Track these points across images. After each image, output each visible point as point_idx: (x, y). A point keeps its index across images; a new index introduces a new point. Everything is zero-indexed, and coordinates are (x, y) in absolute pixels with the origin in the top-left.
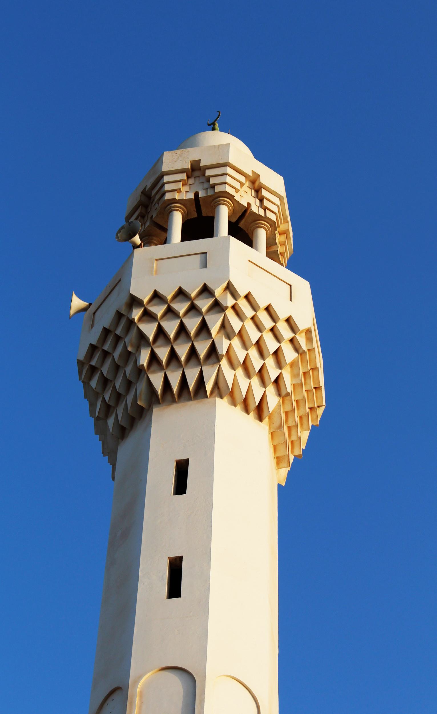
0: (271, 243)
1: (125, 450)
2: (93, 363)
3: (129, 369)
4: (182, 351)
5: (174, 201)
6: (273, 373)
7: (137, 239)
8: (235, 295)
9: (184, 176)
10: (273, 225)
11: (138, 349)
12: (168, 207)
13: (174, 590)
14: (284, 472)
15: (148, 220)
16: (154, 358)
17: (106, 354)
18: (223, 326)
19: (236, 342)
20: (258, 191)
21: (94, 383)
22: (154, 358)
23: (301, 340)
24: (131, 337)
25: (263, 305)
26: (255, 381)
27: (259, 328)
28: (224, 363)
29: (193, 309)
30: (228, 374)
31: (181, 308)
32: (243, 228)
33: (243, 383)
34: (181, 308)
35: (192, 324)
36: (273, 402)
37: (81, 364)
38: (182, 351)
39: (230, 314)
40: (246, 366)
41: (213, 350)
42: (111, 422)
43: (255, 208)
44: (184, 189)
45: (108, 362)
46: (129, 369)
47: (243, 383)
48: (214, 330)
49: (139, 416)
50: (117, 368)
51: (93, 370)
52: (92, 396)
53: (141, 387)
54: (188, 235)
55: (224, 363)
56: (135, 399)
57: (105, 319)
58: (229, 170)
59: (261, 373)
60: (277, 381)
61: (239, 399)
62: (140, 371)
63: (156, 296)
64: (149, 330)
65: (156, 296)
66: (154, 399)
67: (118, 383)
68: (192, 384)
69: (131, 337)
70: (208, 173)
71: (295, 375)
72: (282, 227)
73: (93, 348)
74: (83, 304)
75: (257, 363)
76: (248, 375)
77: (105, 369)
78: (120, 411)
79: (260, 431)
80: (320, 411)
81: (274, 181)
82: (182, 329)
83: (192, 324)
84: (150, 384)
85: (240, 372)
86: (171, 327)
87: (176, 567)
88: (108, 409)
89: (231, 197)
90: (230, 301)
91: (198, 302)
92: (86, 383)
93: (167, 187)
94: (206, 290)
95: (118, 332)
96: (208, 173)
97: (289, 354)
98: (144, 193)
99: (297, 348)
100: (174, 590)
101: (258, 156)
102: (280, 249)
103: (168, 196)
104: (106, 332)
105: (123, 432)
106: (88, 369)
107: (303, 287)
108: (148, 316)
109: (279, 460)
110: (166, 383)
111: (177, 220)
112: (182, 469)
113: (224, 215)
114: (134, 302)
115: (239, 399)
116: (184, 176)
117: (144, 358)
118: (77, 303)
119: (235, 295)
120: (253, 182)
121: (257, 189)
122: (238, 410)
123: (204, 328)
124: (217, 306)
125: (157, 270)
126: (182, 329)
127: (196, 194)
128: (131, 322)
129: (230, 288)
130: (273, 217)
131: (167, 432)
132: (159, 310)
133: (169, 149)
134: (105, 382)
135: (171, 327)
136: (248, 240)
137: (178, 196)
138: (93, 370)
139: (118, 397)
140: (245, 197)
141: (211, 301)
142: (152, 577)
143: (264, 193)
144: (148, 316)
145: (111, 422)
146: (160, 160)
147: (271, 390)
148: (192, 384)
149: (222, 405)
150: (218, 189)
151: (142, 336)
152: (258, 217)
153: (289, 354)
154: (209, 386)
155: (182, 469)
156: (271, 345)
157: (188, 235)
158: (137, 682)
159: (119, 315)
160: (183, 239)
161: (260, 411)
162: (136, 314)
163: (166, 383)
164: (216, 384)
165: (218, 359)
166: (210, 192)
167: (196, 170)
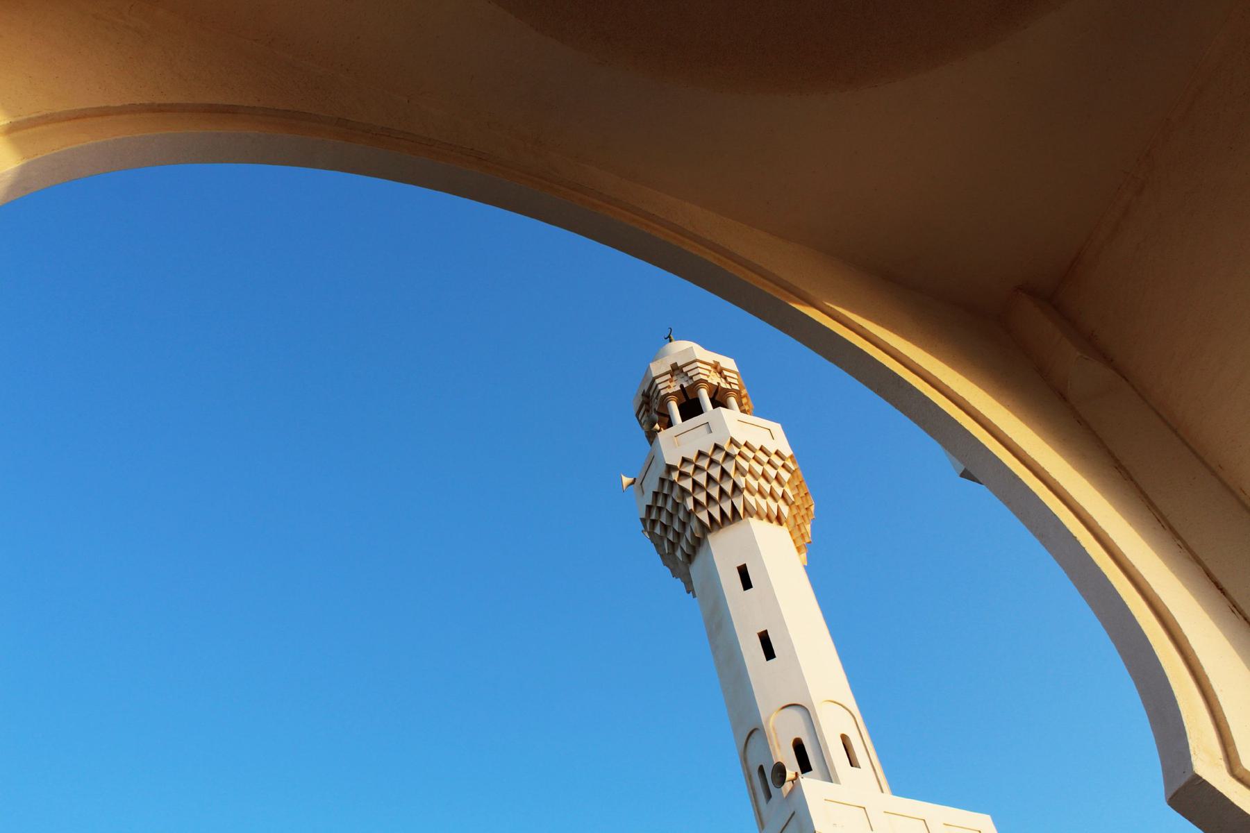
0: (740, 405)
1: (695, 570)
2: (653, 517)
3: (681, 515)
4: (715, 492)
5: (668, 394)
6: (779, 491)
7: (657, 426)
8: (737, 445)
9: (669, 376)
10: (738, 392)
11: (683, 499)
12: (664, 401)
13: (769, 653)
14: (804, 555)
15: (653, 412)
16: (696, 502)
17: (660, 509)
18: (737, 469)
19: (749, 477)
20: (720, 373)
21: (658, 530)
22: (696, 502)
23: (789, 463)
24: (676, 493)
25: (758, 447)
26: (769, 500)
27: (759, 462)
28: (746, 493)
29: (712, 462)
30: (752, 500)
31: (704, 463)
32: (719, 399)
33: (763, 503)
34: (704, 463)
35: (716, 473)
36: (785, 510)
37: (643, 521)
38: (715, 492)
39: (739, 459)
40: (760, 492)
41: (735, 486)
42: (679, 554)
43: (724, 385)
44: (672, 384)
45: (664, 514)
46: (681, 515)
47: (763, 503)
48: (732, 471)
49: (698, 543)
50: (671, 516)
51: (654, 522)
52: (657, 542)
53: (694, 524)
54: (685, 416)
55: (746, 493)
56: (693, 534)
57: (652, 485)
58: (699, 364)
59: (772, 494)
60: (783, 497)
61: (764, 515)
62: (689, 514)
63: (684, 460)
64: (687, 484)
65: (684, 460)
66: (705, 530)
67: (676, 526)
68: (717, 516)
69: (676, 493)
70: (685, 370)
71: (792, 490)
72: (744, 392)
73: (649, 508)
74: (631, 480)
75: (767, 487)
76: (764, 497)
77: (664, 519)
78: (684, 544)
79: (783, 531)
80: (812, 508)
81: (728, 363)
82: (710, 478)
83: (716, 473)
84: (700, 521)
85: (758, 496)
86: (701, 478)
87: (765, 639)
88: (673, 545)
89: (706, 381)
90: (736, 451)
91: (714, 457)
92: (652, 534)
93: (660, 387)
94: (717, 447)
95: (665, 492)
96: (685, 370)
97: (786, 476)
98: (644, 394)
99: (788, 470)
100: (769, 653)
101: (707, 347)
102: (747, 408)
103: (663, 393)
104: (656, 494)
105: (689, 558)
106: (649, 522)
107: (777, 428)
108: (683, 475)
109: (799, 549)
110: (711, 516)
111: (674, 408)
112: (743, 572)
113: (704, 395)
114: (670, 468)
115: (764, 515)
116: (669, 376)
117: (690, 504)
118: (626, 480)
119: (737, 445)
120: (715, 368)
121: (720, 371)
122: (765, 522)
123: (724, 473)
124: (728, 456)
125: (679, 442)
126: (710, 478)
127: (682, 386)
128: (673, 483)
129: (732, 441)
130: (736, 387)
131: (724, 550)
132: (689, 469)
133: (654, 360)
134: (665, 528)
135: (701, 478)
136: (725, 406)
137: (670, 391)
138: (654, 522)
139: (678, 535)
140: (715, 379)
141: (723, 454)
142: (751, 650)
143: (726, 373)
144: (683, 475)
145: (679, 554)
146: (649, 368)
147: (781, 503)
148: (717, 516)
149: (753, 521)
150: (695, 379)
151: (683, 490)
152: (727, 390)
153: (786, 476)
154: (741, 511)
155: (743, 572)
156: (772, 473)
157: (685, 416)
158: (767, 722)
159: (662, 480)
160: (684, 419)
161: (779, 519)
162: (675, 476)
163: (711, 516)
164: (745, 508)
165: (741, 491)
166: (691, 382)
167: (676, 370)
